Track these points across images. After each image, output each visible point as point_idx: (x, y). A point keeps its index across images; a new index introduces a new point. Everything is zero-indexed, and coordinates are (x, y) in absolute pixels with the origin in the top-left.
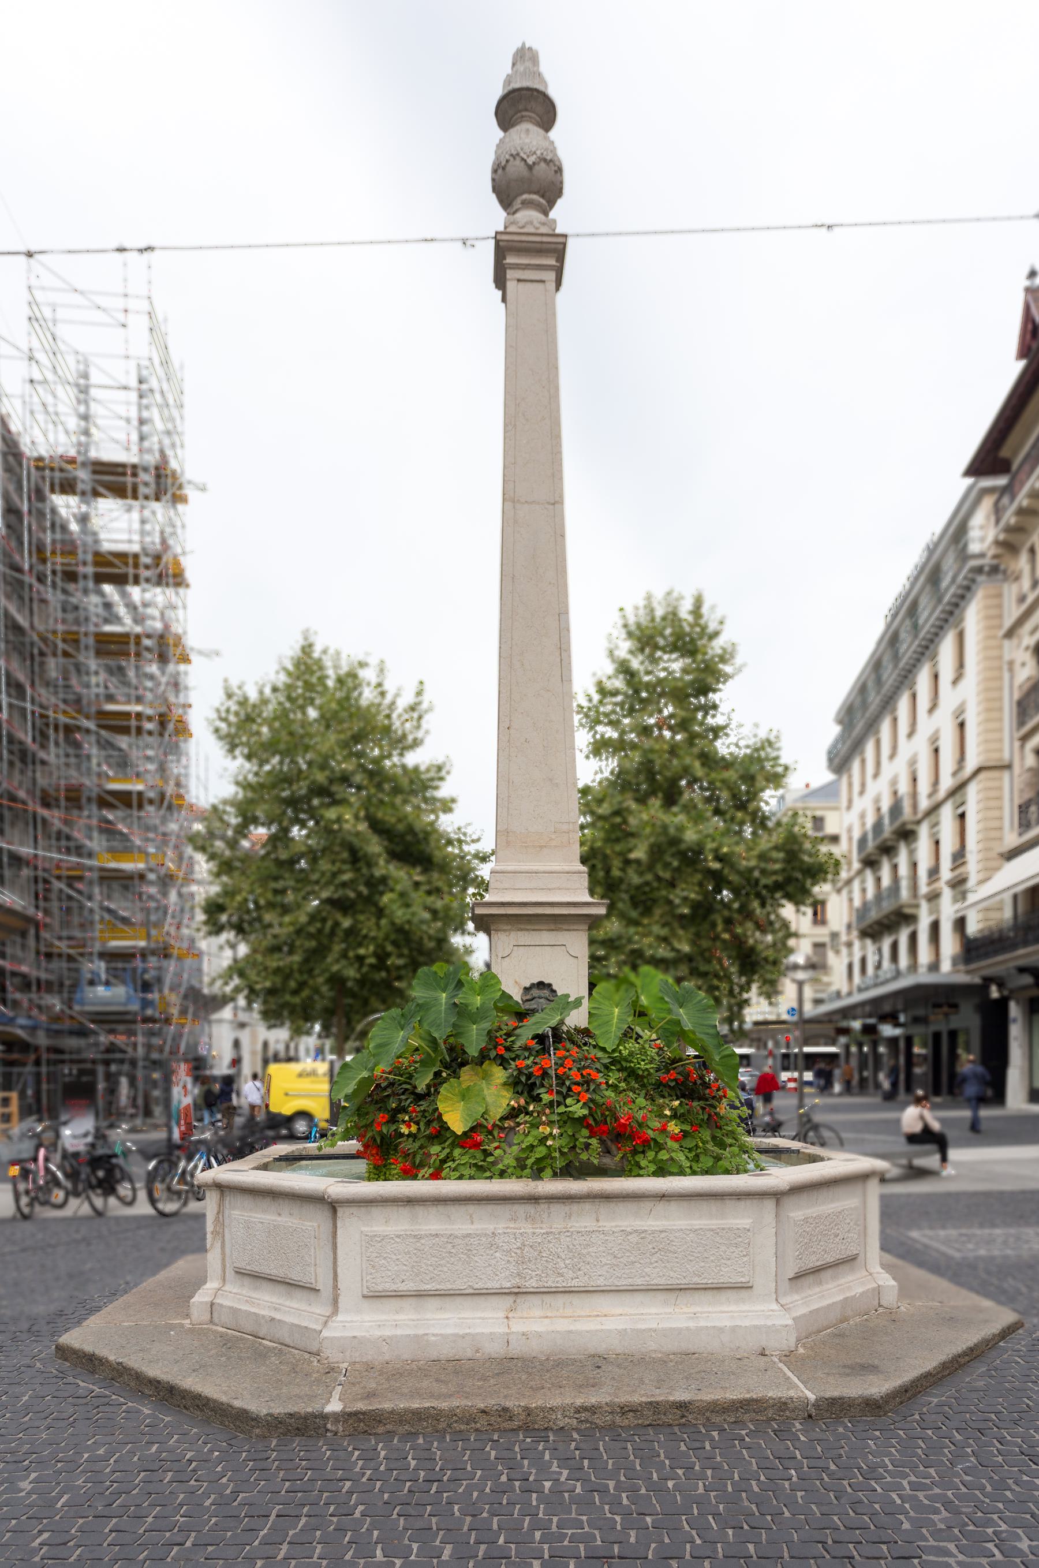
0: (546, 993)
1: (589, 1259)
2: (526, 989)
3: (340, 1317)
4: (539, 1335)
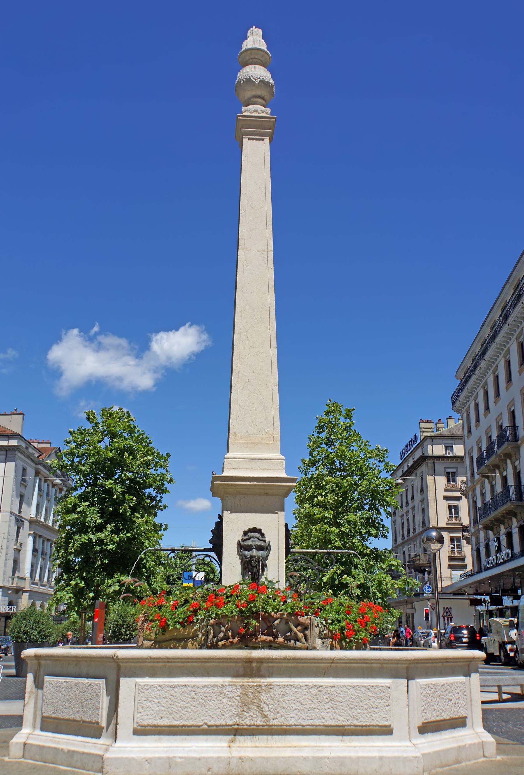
0: (257, 535)
1: (284, 705)
2: (244, 532)
3: (118, 744)
4: (251, 759)
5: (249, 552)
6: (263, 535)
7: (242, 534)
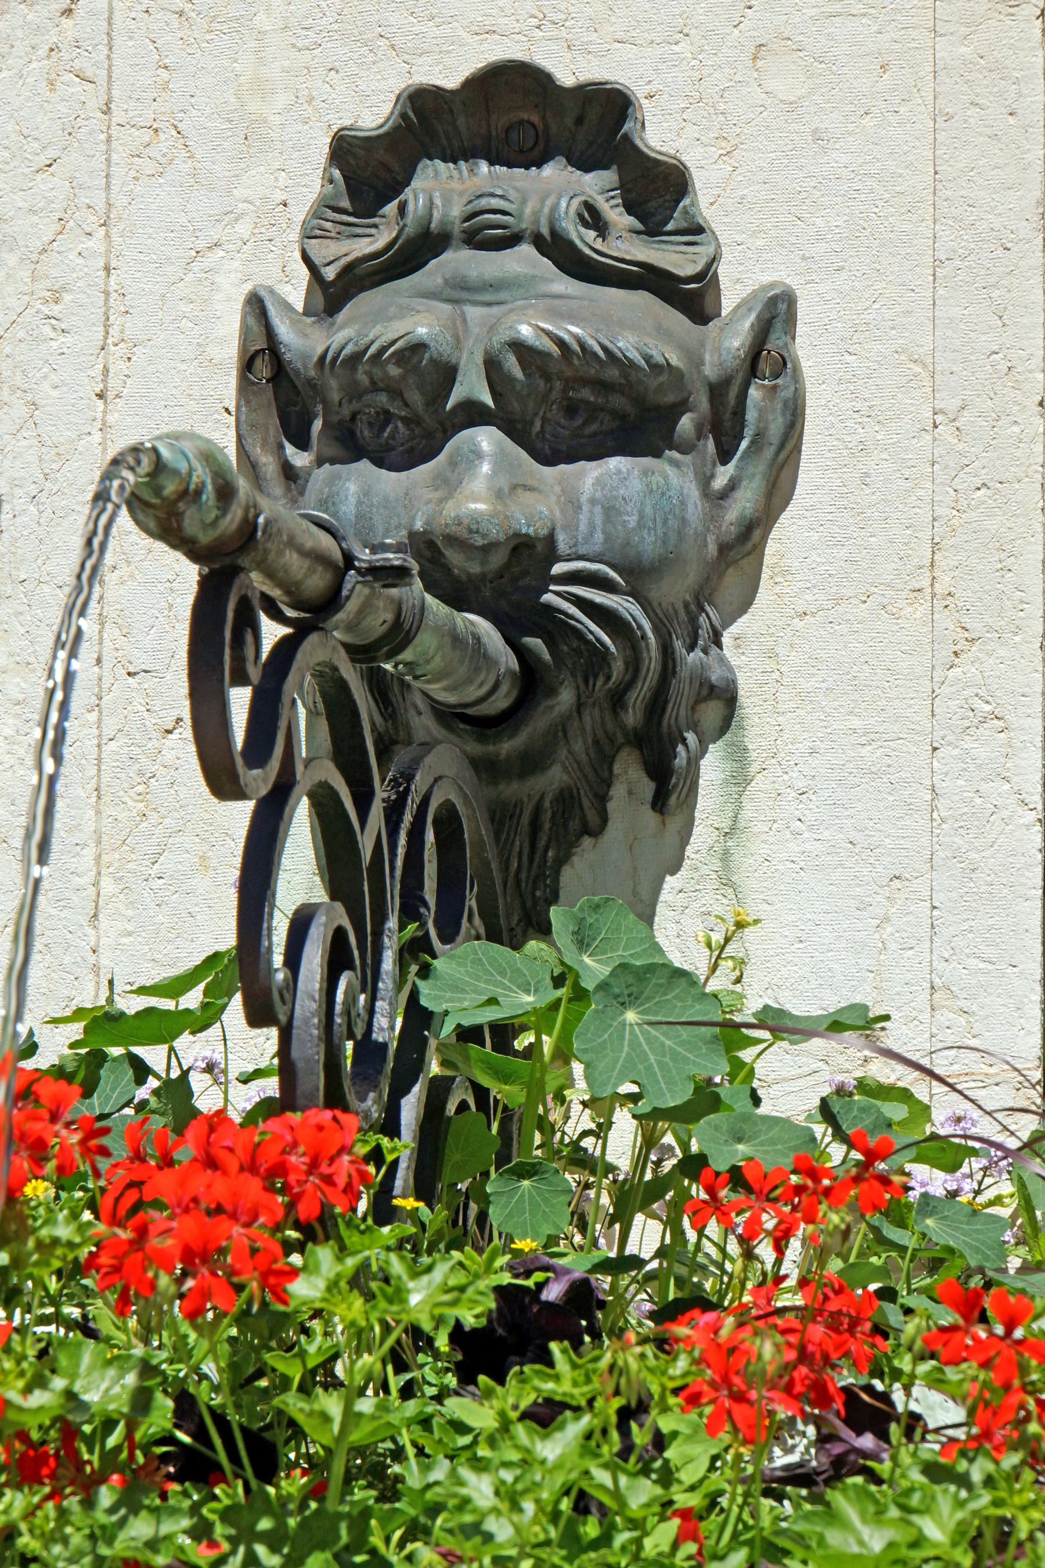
0: (556, 190)
2: (345, 150)
5: (388, 480)
6: (657, 191)
7: (306, 178)
